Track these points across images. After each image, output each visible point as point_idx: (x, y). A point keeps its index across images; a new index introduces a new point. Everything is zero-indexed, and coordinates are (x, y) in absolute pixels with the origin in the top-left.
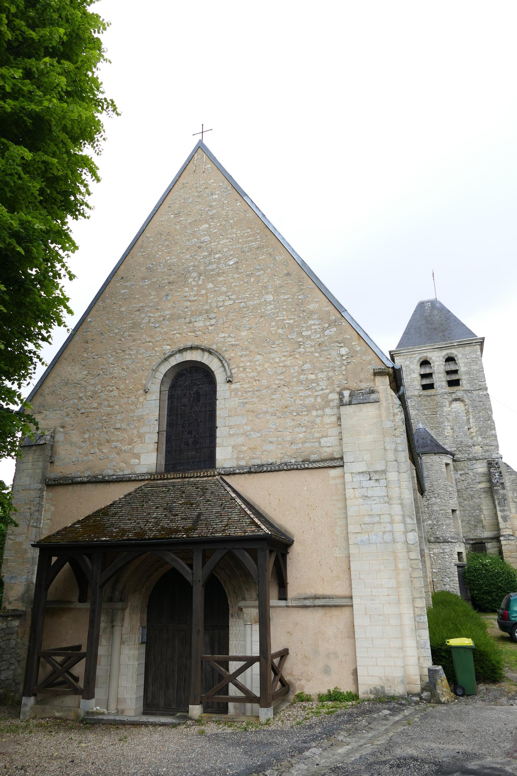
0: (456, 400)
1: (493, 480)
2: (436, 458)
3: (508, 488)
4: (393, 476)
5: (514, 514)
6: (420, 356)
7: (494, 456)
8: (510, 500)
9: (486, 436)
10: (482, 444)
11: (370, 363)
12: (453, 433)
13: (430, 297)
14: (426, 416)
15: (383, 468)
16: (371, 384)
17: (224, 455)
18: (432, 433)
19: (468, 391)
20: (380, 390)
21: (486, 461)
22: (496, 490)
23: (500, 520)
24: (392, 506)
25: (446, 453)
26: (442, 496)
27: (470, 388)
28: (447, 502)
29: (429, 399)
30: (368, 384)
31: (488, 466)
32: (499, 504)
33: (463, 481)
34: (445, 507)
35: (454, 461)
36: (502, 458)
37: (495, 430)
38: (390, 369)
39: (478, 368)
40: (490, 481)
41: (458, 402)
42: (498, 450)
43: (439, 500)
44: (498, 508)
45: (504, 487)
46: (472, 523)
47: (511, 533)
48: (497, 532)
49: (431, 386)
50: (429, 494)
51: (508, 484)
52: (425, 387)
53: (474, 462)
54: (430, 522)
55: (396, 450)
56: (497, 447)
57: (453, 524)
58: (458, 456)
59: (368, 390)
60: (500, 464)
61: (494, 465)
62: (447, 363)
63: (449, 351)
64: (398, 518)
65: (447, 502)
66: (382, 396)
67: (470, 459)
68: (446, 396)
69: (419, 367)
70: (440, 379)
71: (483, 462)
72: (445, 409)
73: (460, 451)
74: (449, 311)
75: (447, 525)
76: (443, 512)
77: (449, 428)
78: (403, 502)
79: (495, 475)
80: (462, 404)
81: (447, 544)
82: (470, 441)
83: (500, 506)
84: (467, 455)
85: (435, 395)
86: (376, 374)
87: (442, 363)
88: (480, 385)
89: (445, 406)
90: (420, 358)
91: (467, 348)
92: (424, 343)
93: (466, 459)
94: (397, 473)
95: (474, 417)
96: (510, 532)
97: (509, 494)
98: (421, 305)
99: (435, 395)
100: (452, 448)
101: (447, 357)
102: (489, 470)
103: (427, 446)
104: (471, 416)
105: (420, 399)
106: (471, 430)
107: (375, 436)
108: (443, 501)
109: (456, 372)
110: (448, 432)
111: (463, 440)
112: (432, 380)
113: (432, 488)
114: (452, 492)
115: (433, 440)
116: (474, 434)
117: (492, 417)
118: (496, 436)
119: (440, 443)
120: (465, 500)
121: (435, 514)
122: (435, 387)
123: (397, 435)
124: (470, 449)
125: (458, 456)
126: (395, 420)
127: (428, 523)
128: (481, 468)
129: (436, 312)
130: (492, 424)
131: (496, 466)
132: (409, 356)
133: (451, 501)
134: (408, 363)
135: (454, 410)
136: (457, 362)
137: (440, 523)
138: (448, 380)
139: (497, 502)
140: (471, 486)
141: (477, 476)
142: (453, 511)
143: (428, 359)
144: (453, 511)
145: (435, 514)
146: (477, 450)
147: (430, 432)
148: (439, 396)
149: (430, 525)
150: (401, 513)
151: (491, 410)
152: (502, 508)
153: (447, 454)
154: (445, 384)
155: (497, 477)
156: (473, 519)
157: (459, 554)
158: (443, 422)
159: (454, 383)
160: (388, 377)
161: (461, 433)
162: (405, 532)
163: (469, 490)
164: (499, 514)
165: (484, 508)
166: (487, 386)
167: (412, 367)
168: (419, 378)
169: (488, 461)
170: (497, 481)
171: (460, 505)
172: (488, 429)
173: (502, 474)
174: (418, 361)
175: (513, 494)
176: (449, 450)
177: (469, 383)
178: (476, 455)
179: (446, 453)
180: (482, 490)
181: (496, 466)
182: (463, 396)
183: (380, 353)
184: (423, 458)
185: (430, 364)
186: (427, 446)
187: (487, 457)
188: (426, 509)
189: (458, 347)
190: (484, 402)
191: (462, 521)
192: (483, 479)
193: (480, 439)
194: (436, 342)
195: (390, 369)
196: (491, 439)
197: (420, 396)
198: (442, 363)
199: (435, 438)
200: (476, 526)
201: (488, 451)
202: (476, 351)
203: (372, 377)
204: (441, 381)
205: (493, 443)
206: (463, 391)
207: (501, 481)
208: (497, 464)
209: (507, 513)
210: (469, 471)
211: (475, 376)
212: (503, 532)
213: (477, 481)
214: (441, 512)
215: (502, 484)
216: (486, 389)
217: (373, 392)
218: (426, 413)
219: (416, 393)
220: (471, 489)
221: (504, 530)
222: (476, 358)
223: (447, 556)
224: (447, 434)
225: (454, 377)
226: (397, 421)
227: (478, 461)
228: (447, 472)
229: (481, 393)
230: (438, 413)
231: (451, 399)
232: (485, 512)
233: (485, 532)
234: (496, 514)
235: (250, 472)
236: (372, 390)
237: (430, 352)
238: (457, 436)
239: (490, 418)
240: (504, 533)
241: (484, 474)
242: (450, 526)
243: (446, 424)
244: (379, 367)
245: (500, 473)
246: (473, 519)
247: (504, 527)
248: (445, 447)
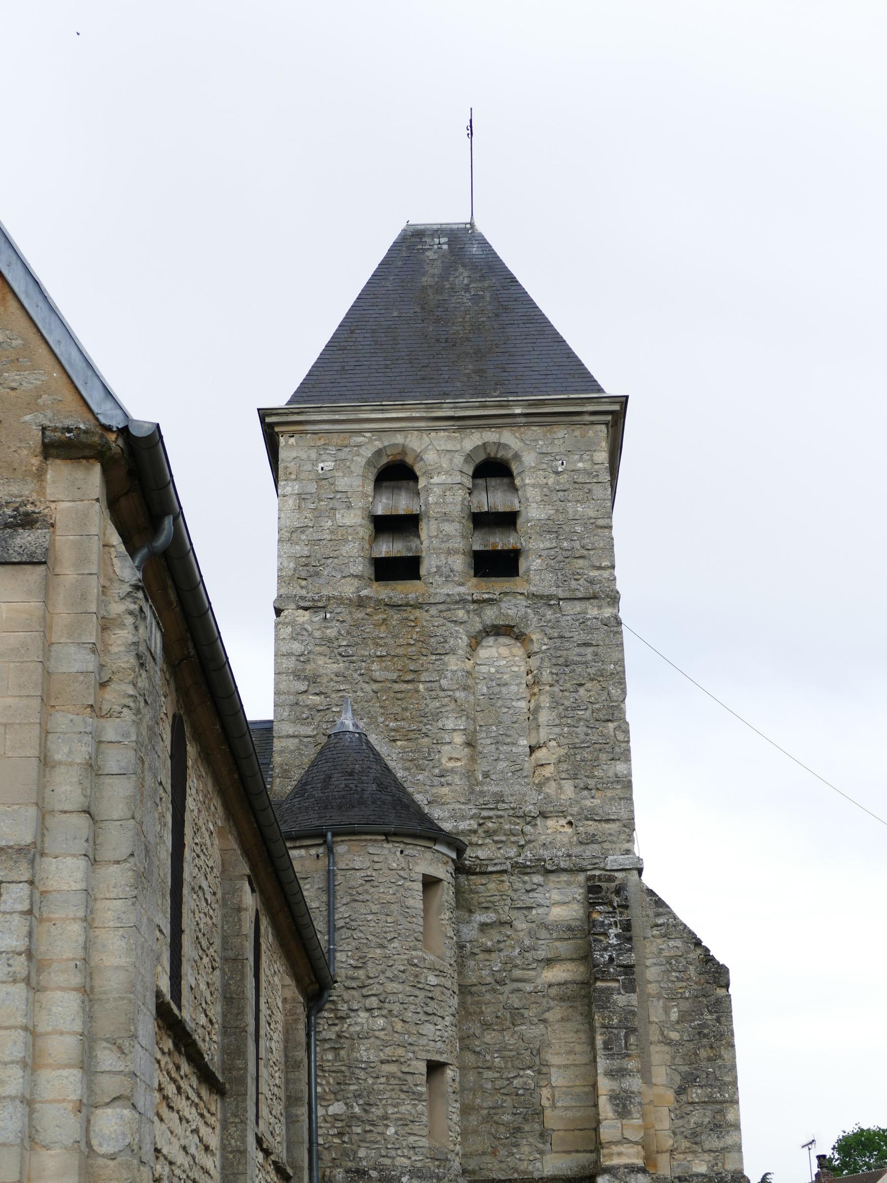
0: (498, 631)
1: (597, 955)
2: (387, 857)
3: (652, 988)
4: (65, 873)
5: (660, 1090)
6: (378, 445)
7: (614, 860)
8: (654, 1036)
9: (591, 783)
10: (575, 810)
11: (32, 405)
12: (473, 759)
13: (446, 212)
14: (375, 686)
15: (27, 838)
16: (26, 490)
18: (392, 755)
19: (546, 600)
20: (59, 519)
21: (581, 877)
22: (602, 990)
23: (605, 1108)
24: (40, 996)
25: (429, 833)
26: (396, 1008)
27: (553, 590)
28: (414, 1030)
29: (396, 617)
30: (15, 490)
31: (587, 899)
32: (607, 1046)
33: (489, 951)
34: (400, 1051)
35: (460, 869)
36: (640, 871)
37: (628, 760)
38: (112, 437)
39: (592, 514)
40: (586, 958)
41: (503, 640)
42: (630, 839)
43: (381, 1022)
44: (602, 1064)
45: (632, 982)
46: (506, 1118)
47: (639, 1162)
48: (592, 1156)
49: (405, 569)
50: (346, 995)
51: (652, 973)
52: (389, 570)
53: (537, 879)
54: (337, 1108)
55: (93, 769)
56: (629, 825)
57: (424, 1119)
58: (482, 854)
59: (8, 511)
60: (631, 892)
61: (615, 901)
62: (481, 482)
63: (490, 436)
64: (62, 1046)
65: (414, 1030)
66: (64, 541)
67: (522, 869)
68: (461, 614)
69: (370, 488)
70: (444, 545)
71: (569, 884)
72: (453, 663)
73: (489, 834)
74: (513, 280)
75: (404, 1122)
76: (393, 1068)
77: (459, 739)
78: (97, 982)
79: (606, 934)
80: (518, 650)
82: (533, 796)
83: (610, 1057)
84: (512, 852)
85: (418, 606)
86: (60, 447)
87: (458, 478)
88: (591, 582)
89: (453, 651)
90: (379, 453)
91: (561, 432)
92: (402, 394)
93: (508, 866)
94: (82, 863)
95: (556, 703)
96: (637, 1155)
97: (652, 1011)
98: (412, 243)
99: (418, 606)
100: (463, 818)
101: (482, 457)
102: (589, 916)
103: (361, 802)
104: (545, 701)
105: (359, 615)
106: (541, 754)
107: (9, 701)
108: (399, 1026)
109: (508, 520)
110: (452, 753)
111: (507, 791)
112: (414, 543)
113: (361, 973)
114: (437, 993)
115: (387, 780)
116: (548, 771)
117: (622, 711)
118: (629, 785)
119: (419, 798)
120: (487, 1026)
121: (362, 1075)
122: (423, 571)
123: (106, 707)
124: (528, 829)
125: (481, 852)
126: (106, 645)
127: (332, 1110)
128: (561, 903)
129: (463, 276)
130: (621, 736)
131: (616, 901)
132: (336, 439)
133: (428, 1029)
134: (329, 465)
135: (484, 669)
136: (518, 482)
137: (377, 1112)
138: (476, 547)
139: (599, 1040)
140: (517, 973)
141: (543, 934)
142: (434, 1068)
143: (409, 460)
144: (434, 1068)
145: (362, 1075)
146: (555, 834)
147: (382, 749)
148: (433, 611)
149: (336, 1118)
150: (78, 1026)
151: (621, 683)
152: (616, 1064)
153: (435, 840)
154: (459, 563)
155: (614, 941)
156: (508, 1102)
158: (437, 716)
159: (496, 565)
160: (97, 469)
161: (502, 765)
162: (86, 1107)
163: (507, 989)
164: (605, 1085)
165: (554, 1060)
166: (619, 586)
167: (342, 483)
168: (365, 530)
169: (589, 878)
170: (611, 959)
171: (464, 1048)
172: (603, 757)
173: (636, 931)
174: (369, 463)
176: (447, 826)
177: (554, 571)
178: (546, 854)
179: (429, 833)
180: (553, 991)
181: (616, 901)
182: (525, 617)
183: (81, 364)
184: (340, 849)
185: (415, 478)
186: (361, 802)
187: (585, 864)
188: (330, 1056)
189: (528, 425)
190: (600, 650)
191: (466, 1111)
192: (564, 948)
193: (568, 788)
194: (446, 395)
195: (112, 437)
196: (609, 794)
197: (361, 602)
198: (458, 478)
199: (400, 774)
200: (518, 1129)
201: (592, 839)
202: (590, 448)
203: (36, 461)
204: (449, 552)
205: (613, 810)
206: (528, 597)
207: (624, 960)
208: (618, 891)
209: (635, 1083)
210: (515, 914)
211: (577, 545)
212: (611, 1155)
213: (542, 954)
214: (387, 1068)
215: (628, 969)
216: (614, 599)
217: (27, 521)
218: (377, 675)
219: (349, 589)
220: (516, 985)
221: (615, 1149)
222: (589, 473)
224: (451, 765)
225: (500, 541)
226: (114, 649)
227: (552, 877)
228: (426, 910)
229: (593, 612)
230: (424, 676)
231: (479, 626)
232: (557, 1078)
233: (548, 1157)
234: (595, 1086)
236: (27, 514)
237: (419, 430)
238: (486, 775)
239: (614, 713)
240: (616, 1161)
241: (570, 929)
242: (415, 1128)
243: (450, 724)
244: (68, 422)
245: (627, 927)
246: (508, 1102)
247: (617, 1136)
248: (436, 813)
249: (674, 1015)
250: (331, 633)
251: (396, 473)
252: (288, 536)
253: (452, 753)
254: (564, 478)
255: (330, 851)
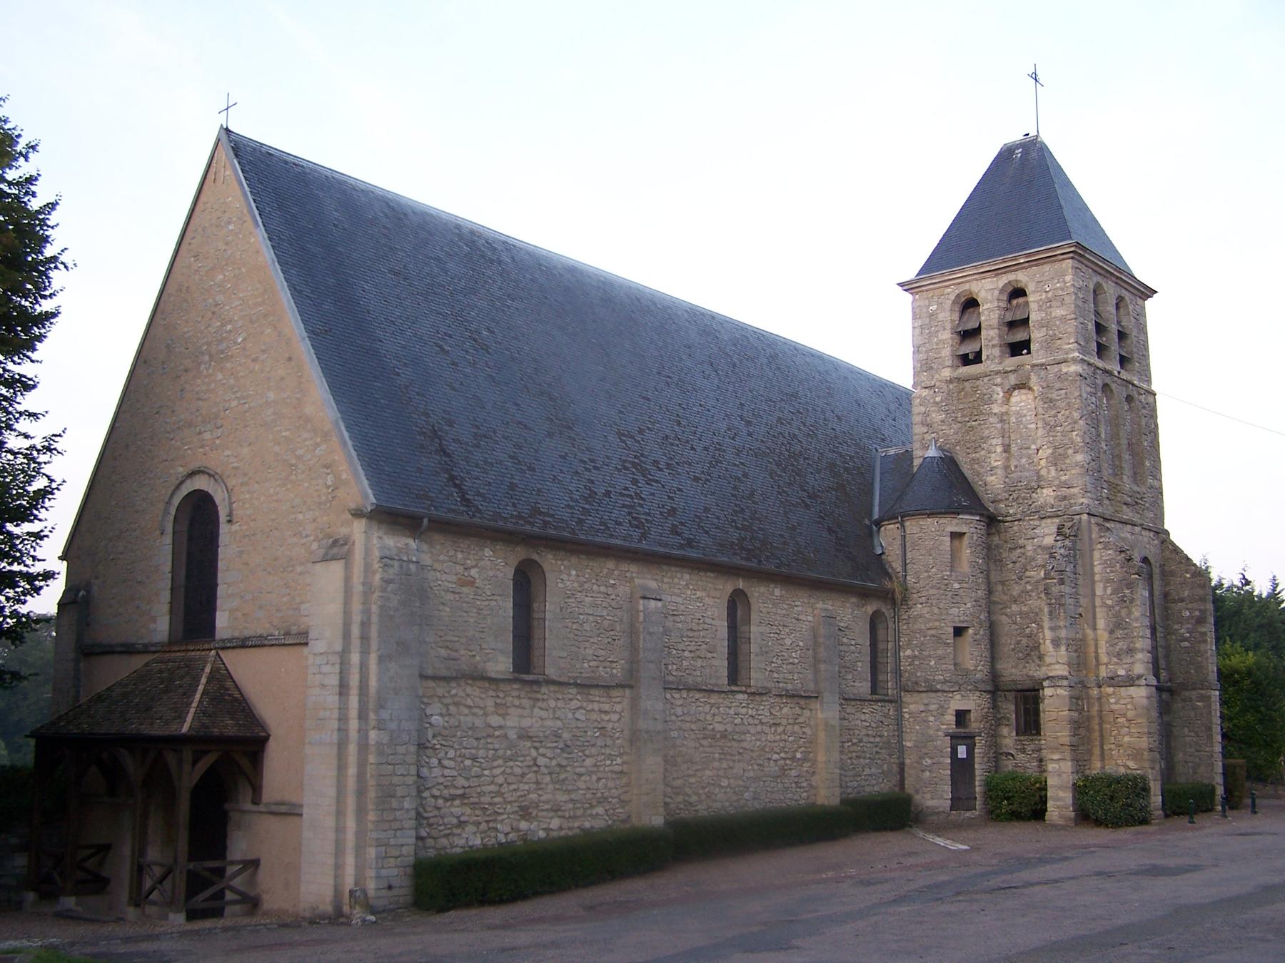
17: (224, 623)
34: (937, 624)
39: (1064, 313)
52: (966, 360)
54: (908, 652)
63: (1012, 277)
70: (991, 338)
72: (996, 409)
76: (933, 632)
77: (999, 449)
81: (933, 695)
90: (958, 296)
91: (1047, 267)
98: (1005, 155)
134: (934, 308)
142: (959, 632)
157: (961, 716)
161: (1024, 460)
174: (954, 302)
175: (1105, 588)
184: (907, 524)
223: (932, 719)
225: (1020, 336)
235: (243, 647)
249: (1109, 591)
250: (938, 399)
251: (970, 304)
252: (917, 350)
253: (996, 460)
254: (1050, 295)
255: (903, 526)
